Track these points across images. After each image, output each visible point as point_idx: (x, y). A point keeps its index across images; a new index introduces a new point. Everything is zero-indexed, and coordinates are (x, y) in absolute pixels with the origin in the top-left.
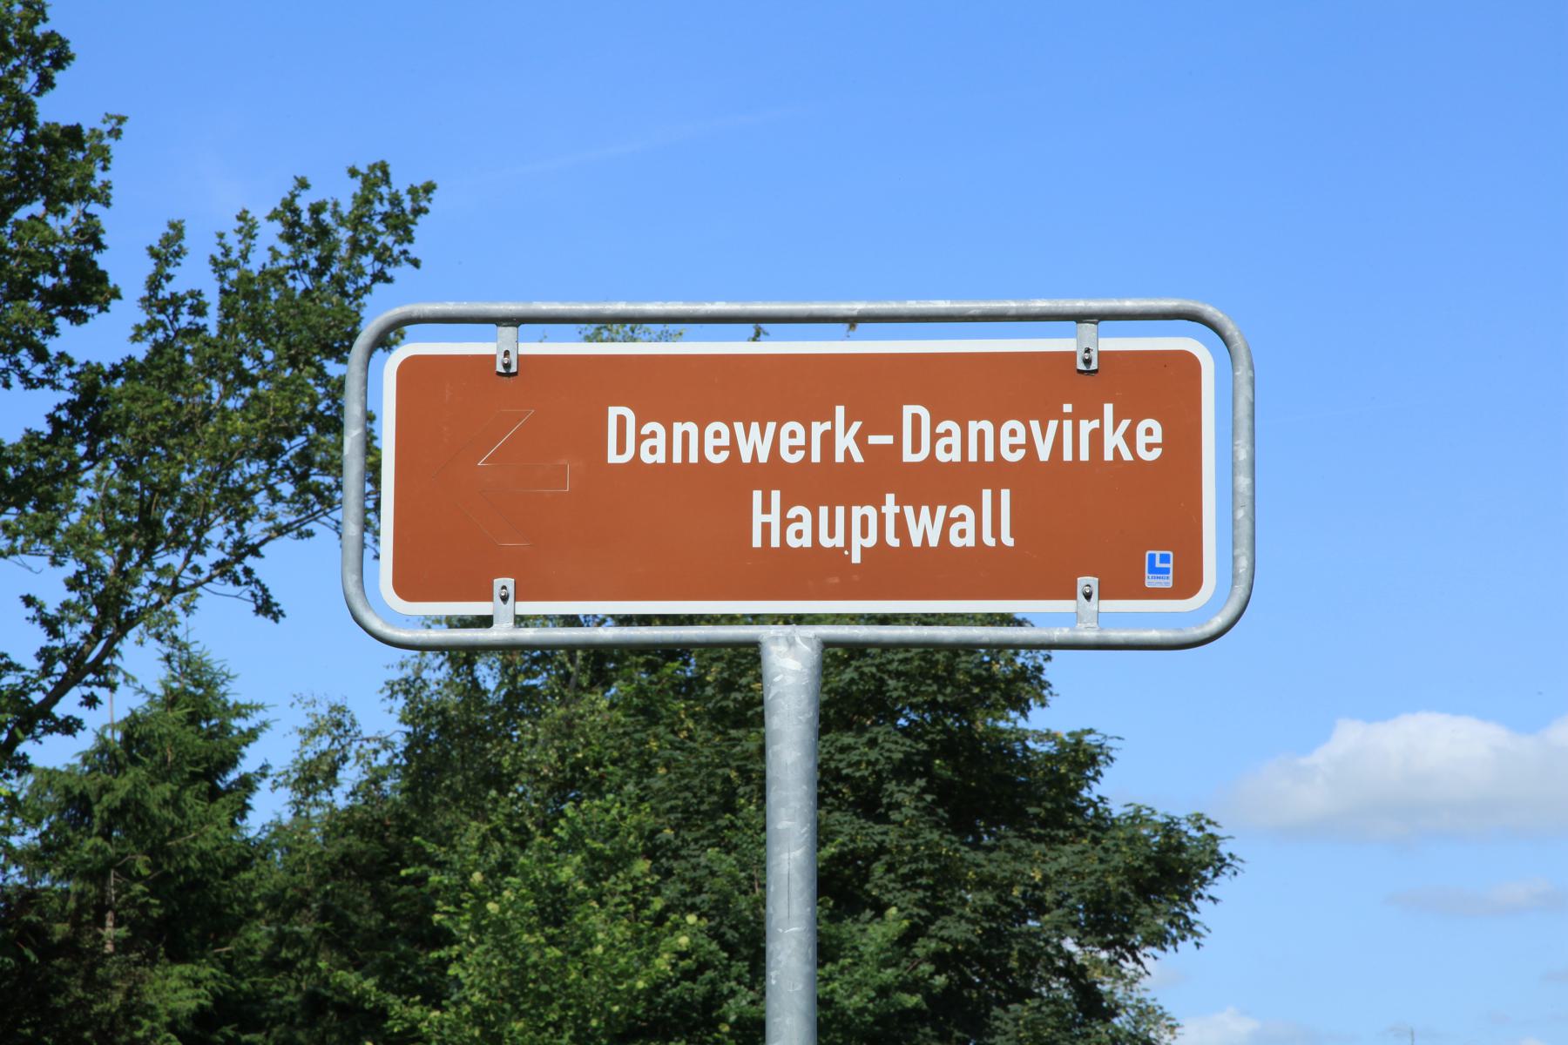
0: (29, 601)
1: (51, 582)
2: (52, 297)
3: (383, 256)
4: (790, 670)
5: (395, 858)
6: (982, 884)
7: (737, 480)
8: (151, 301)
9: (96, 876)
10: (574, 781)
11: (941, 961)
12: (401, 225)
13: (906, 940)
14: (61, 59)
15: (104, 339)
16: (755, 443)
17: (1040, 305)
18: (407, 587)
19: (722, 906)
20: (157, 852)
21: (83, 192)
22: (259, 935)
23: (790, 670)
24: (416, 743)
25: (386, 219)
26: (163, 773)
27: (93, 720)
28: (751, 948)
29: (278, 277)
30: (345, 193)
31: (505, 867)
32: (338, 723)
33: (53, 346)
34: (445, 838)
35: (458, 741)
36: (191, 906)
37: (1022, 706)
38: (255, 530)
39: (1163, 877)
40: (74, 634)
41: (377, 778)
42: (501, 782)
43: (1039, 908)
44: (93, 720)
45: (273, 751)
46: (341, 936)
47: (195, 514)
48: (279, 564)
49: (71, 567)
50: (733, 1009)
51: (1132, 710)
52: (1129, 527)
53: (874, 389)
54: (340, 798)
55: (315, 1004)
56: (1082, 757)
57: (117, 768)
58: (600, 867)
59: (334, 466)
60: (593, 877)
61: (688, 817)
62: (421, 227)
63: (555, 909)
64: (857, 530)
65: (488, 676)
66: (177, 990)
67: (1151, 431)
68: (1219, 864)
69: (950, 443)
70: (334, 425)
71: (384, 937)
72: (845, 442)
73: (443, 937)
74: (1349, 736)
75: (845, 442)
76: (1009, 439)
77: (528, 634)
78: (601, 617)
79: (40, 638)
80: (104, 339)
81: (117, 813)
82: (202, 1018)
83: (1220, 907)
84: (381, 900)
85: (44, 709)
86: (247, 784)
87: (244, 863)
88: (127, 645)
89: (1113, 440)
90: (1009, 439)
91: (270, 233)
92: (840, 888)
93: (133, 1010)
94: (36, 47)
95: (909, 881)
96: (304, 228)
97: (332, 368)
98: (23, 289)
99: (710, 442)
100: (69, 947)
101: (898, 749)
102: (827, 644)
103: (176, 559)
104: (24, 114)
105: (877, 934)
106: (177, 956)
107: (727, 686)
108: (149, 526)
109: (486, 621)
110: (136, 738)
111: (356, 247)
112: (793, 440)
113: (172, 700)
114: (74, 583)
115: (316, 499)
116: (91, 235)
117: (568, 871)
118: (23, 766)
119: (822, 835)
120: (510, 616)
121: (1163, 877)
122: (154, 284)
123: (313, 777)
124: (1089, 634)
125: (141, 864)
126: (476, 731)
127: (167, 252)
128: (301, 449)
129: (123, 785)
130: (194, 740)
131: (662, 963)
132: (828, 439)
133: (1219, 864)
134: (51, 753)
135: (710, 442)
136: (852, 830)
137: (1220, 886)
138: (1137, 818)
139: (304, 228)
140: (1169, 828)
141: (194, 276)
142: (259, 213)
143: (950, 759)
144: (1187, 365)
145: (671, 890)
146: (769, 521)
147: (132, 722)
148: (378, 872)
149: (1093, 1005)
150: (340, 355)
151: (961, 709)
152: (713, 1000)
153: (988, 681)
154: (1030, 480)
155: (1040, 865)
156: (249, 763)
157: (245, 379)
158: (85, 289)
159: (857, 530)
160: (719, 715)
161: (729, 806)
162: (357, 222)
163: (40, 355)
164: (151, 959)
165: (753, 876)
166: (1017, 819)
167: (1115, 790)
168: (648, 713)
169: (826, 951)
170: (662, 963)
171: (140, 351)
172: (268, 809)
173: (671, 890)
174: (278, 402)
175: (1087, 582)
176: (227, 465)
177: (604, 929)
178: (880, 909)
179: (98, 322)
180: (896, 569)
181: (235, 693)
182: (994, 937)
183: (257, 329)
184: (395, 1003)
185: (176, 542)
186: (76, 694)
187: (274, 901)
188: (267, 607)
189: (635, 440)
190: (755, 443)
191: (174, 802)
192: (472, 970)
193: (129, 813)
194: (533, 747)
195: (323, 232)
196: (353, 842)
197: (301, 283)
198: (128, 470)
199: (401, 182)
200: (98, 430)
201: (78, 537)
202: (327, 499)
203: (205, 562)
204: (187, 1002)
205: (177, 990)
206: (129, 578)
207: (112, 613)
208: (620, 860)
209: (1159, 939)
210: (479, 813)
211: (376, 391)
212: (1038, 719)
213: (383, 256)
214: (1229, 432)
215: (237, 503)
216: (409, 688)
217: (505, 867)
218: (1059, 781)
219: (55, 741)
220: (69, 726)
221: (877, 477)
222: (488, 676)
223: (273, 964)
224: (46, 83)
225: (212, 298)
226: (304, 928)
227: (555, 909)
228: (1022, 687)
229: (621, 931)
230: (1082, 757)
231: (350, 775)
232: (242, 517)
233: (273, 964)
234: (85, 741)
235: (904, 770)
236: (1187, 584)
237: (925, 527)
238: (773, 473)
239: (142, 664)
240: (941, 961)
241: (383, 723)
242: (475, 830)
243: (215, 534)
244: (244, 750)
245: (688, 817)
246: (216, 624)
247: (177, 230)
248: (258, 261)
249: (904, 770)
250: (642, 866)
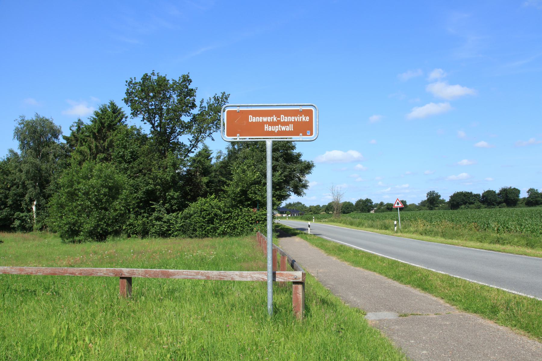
1: (191, 137)
2: (191, 107)
3: (225, 102)
5: (227, 166)
6: (289, 168)
7: (263, 123)
8: (200, 107)
9: (196, 168)
10: (245, 158)
11: (284, 176)
12: (226, 99)
13: (281, 174)
14: (191, 82)
15: (195, 111)
16: (265, 119)
17: (296, 104)
18: (228, 135)
19: (261, 171)
20: (202, 165)
21: (193, 96)
22: (213, 174)
24: (229, 154)
25: (225, 98)
26: (203, 157)
27: (196, 152)
28: (265, 176)
29: (213, 104)
30: (220, 95)
31: (239, 167)
32: (220, 152)
33: (190, 112)
34: (232, 164)
35: (232, 155)
36: (206, 171)
37: (293, 150)
38: (211, 131)
39: (308, 167)
40: (193, 142)
41: (225, 158)
42: (237, 158)
43: (295, 171)
44: (196, 152)
45: (214, 155)
46: (221, 174)
47: (205, 130)
48: (214, 135)
49: (193, 135)
50: (263, 182)
51: (304, 149)
52: (305, 128)
53: (278, 113)
54: (221, 160)
55: (219, 181)
56: (299, 155)
57: (198, 157)
58: (248, 167)
59: (220, 125)
60: (248, 168)
61: (258, 162)
62: (229, 99)
63: (244, 171)
64: (276, 129)
65: (236, 147)
66: (205, 180)
67: (308, 118)
68: (314, 166)
69: (286, 119)
70: (220, 120)
71: (226, 174)
72: (275, 119)
73: (232, 174)
74: (327, 153)
75: (275, 119)
76: (292, 119)
77: (241, 140)
78: (247, 138)
79: (190, 143)
80: (195, 111)
81: (198, 161)
82: (208, 182)
83: (314, 170)
84: (226, 170)
85: (190, 150)
86: (211, 158)
87: (211, 167)
88: (199, 144)
89: (304, 119)
90: (292, 119)
91: (213, 100)
92: (274, 169)
93: (201, 182)
94: (188, 80)
95: (281, 168)
96: (216, 99)
97: (219, 114)
98: (187, 106)
99: (260, 119)
100: (194, 175)
101: (280, 154)
102: (273, 141)
103: (203, 135)
104: (187, 88)
105: (278, 174)
106: (205, 176)
107: (262, 148)
108: (201, 131)
110: (200, 154)
111: (222, 101)
112: (269, 119)
113: (203, 150)
114: (193, 137)
115: (218, 128)
116: (194, 100)
117: (245, 167)
118: (188, 156)
119: (272, 163)
120: (238, 138)
121: (308, 167)
122: (201, 105)
123: (218, 158)
124: (301, 140)
125: (201, 167)
126: (235, 153)
127: (202, 102)
128: (216, 122)
129: (199, 159)
130: (206, 154)
131: (255, 177)
132: (273, 119)
133: (314, 166)
134: (191, 155)
135: (260, 119)
136: (276, 163)
137: (314, 169)
138: (305, 161)
139: (216, 99)
140: (308, 162)
141: (205, 104)
142: (211, 98)
143: (285, 154)
144: (311, 111)
145: (256, 169)
146: (267, 128)
147: (199, 152)
148: (225, 168)
149: (300, 180)
150: (220, 112)
151: (287, 150)
152: (261, 181)
153: (289, 147)
154: (295, 123)
155: (295, 166)
156: (211, 156)
157: (210, 115)
158: (194, 106)
159: (276, 129)
160: (261, 151)
161: (262, 160)
162: (222, 98)
163: (189, 113)
164: (202, 176)
165: (265, 168)
166: (292, 162)
167: (303, 158)
168: (253, 150)
169: (273, 175)
170: (255, 177)
171: (199, 113)
172: (214, 161)
173: (256, 169)
174: (214, 118)
175: (301, 134)
176: (208, 124)
177: (249, 173)
178: (278, 171)
179: (195, 109)
180: (280, 133)
181: (210, 149)
182: (290, 174)
183: (211, 110)
184: (227, 181)
185: (203, 133)
186: (194, 149)
187: (215, 170)
188: (213, 140)
189: (252, 119)
190: (265, 119)
191: (204, 160)
192: (235, 177)
193: (199, 161)
194: (241, 155)
195: (218, 99)
196: (222, 164)
197: (216, 105)
198: (198, 125)
199: (226, 94)
200: (195, 121)
201: (193, 132)
202: (219, 128)
203: (206, 135)
204: (206, 181)
205: (205, 180)
206: (199, 137)
207: (197, 141)
208: (251, 166)
209: (307, 173)
210: (235, 161)
211: (224, 116)
212: (295, 151)
213: (225, 102)
214: (316, 118)
215: (210, 128)
216: (228, 148)
217: (239, 167)
218: (297, 158)
219: (192, 154)
220: (193, 152)
221: (278, 123)
222: (236, 147)
223: (215, 177)
224: (189, 84)
225: (207, 107)
226: (218, 173)
227: (244, 171)
228: (293, 148)
229: (251, 174)
230: (299, 155)
231: (222, 157)
232: (210, 130)
233: (215, 177)
234: (195, 154)
235: (281, 157)
236: (311, 134)
237: (283, 128)
238: (267, 123)
239: (200, 146)
240: (284, 176)
241: (225, 152)
242: (235, 163)
243: (207, 132)
244: (41, 117)
245: (258, 162)
246: (208, 141)
247: (203, 99)
248: (211, 103)
249: (281, 157)
250: (253, 167)
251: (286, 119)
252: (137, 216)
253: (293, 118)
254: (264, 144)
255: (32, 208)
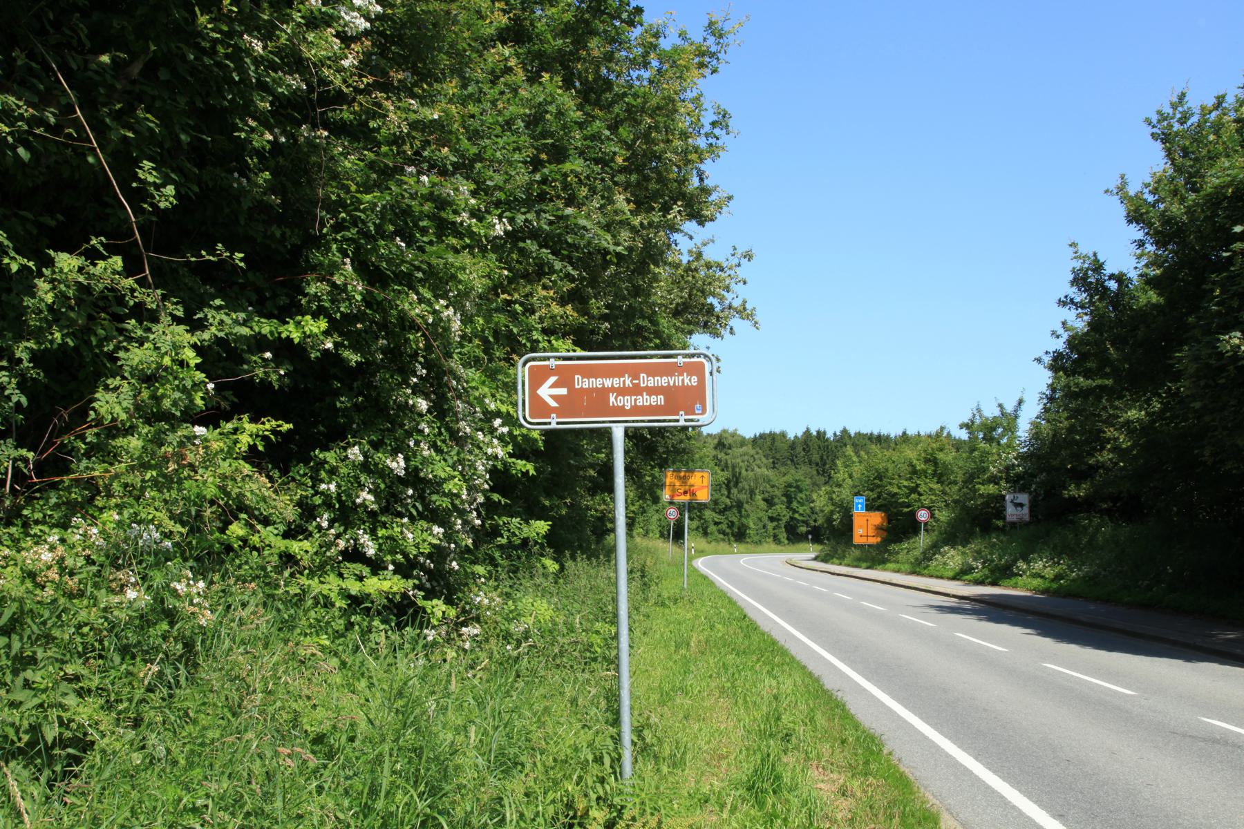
0: (1106, 192)
4: (618, 433)
7: (604, 392)
16: (608, 383)
23: (618, 433)
39: (845, 431)
64: (627, 402)
67: (694, 379)
69: (651, 382)
72: (628, 383)
76: (663, 381)
89: (687, 381)
90: (663, 381)
99: (598, 383)
109: (678, 421)
135: (598, 383)
146: (660, 400)
180: (636, 410)
190: (608, 383)
221: (636, 390)
236: (704, 412)
238: (612, 389)
251: (651, 382)
252: (350, 597)
253: (616, 381)
254: (604, 436)
255: (1117, 349)
